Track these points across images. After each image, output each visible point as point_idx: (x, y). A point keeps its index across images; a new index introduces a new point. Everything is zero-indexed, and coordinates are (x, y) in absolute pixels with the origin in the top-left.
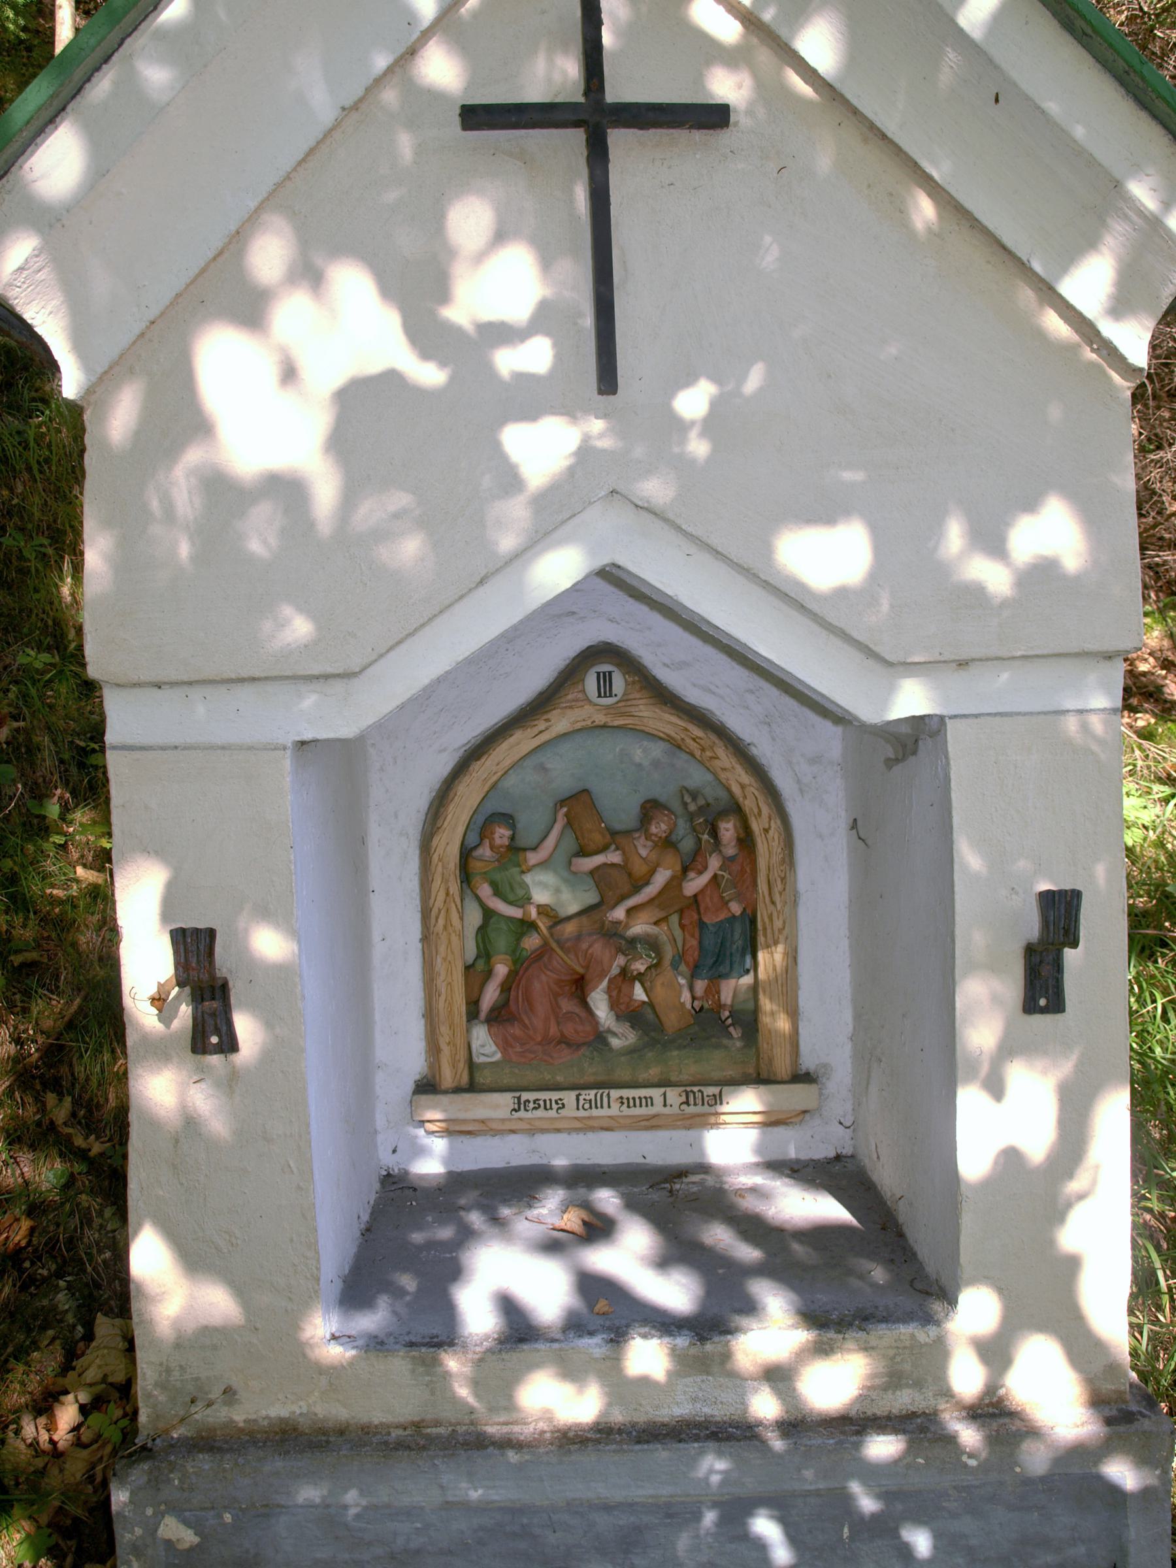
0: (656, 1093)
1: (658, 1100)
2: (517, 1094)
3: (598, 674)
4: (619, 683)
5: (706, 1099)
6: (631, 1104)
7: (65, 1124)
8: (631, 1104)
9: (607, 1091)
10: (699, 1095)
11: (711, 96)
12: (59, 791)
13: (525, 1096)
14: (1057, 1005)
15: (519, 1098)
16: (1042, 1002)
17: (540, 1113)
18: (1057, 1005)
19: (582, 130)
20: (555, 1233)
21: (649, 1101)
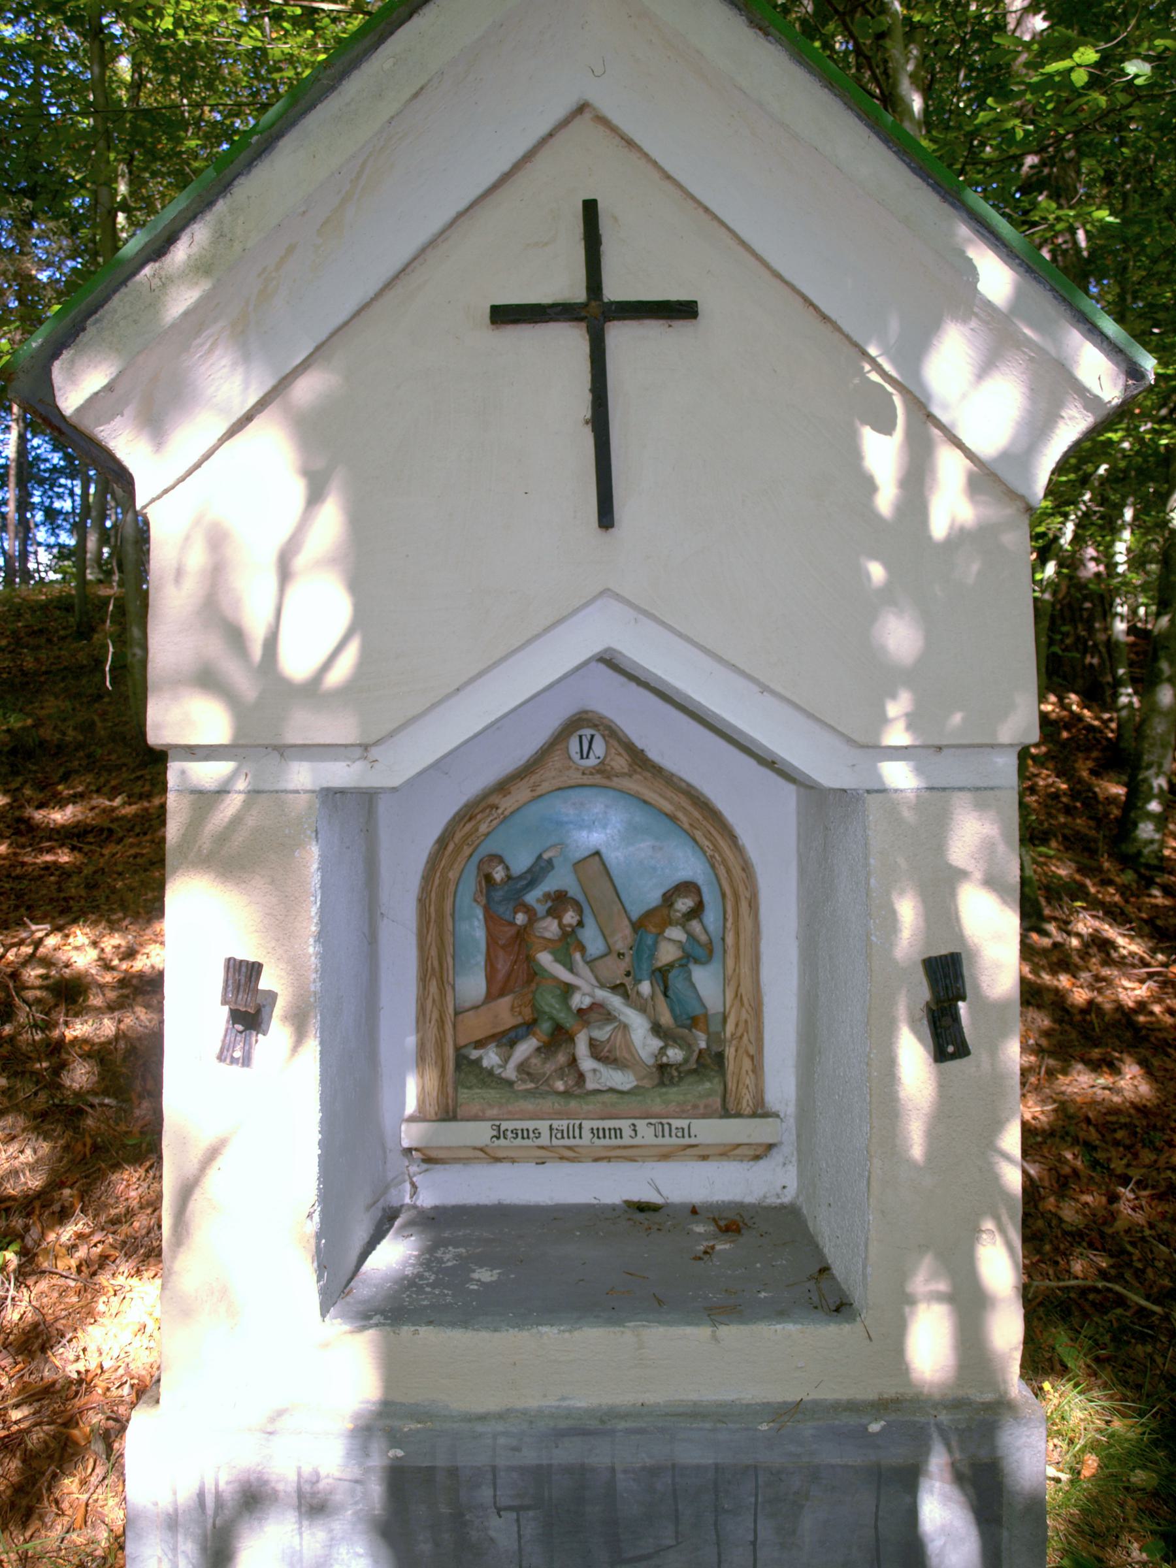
0: (625, 1124)
1: (627, 1132)
2: (497, 1123)
3: (580, 737)
4: (599, 748)
5: (674, 1131)
6: (601, 1135)
7: (183, 772)
8: (601, 1135)
9: (577, 1122)
10: (666, 1127)
11: (174, 872)
12: (24, 35)
13: (505, 1125)
14: (963, 1051)
15: (499, 1126)
16: (951, 1049)
17: (519, 1141)
18: (963, 1051)
19: (606, 300)
20: (954, 1443)
21: (618, 1132)
